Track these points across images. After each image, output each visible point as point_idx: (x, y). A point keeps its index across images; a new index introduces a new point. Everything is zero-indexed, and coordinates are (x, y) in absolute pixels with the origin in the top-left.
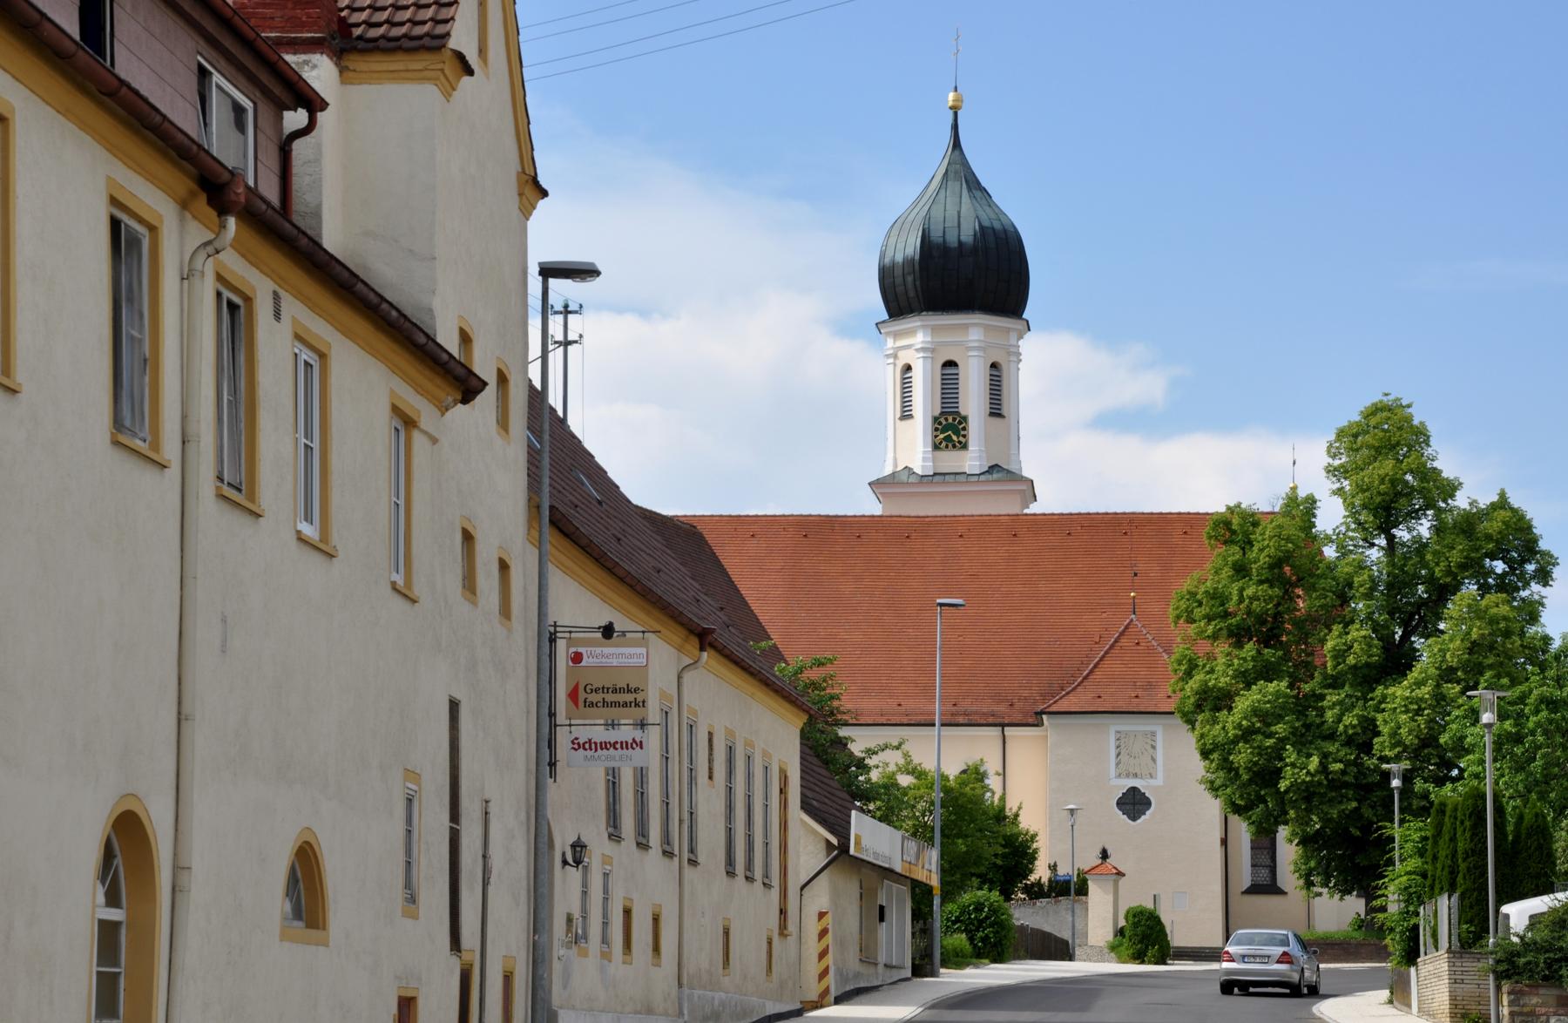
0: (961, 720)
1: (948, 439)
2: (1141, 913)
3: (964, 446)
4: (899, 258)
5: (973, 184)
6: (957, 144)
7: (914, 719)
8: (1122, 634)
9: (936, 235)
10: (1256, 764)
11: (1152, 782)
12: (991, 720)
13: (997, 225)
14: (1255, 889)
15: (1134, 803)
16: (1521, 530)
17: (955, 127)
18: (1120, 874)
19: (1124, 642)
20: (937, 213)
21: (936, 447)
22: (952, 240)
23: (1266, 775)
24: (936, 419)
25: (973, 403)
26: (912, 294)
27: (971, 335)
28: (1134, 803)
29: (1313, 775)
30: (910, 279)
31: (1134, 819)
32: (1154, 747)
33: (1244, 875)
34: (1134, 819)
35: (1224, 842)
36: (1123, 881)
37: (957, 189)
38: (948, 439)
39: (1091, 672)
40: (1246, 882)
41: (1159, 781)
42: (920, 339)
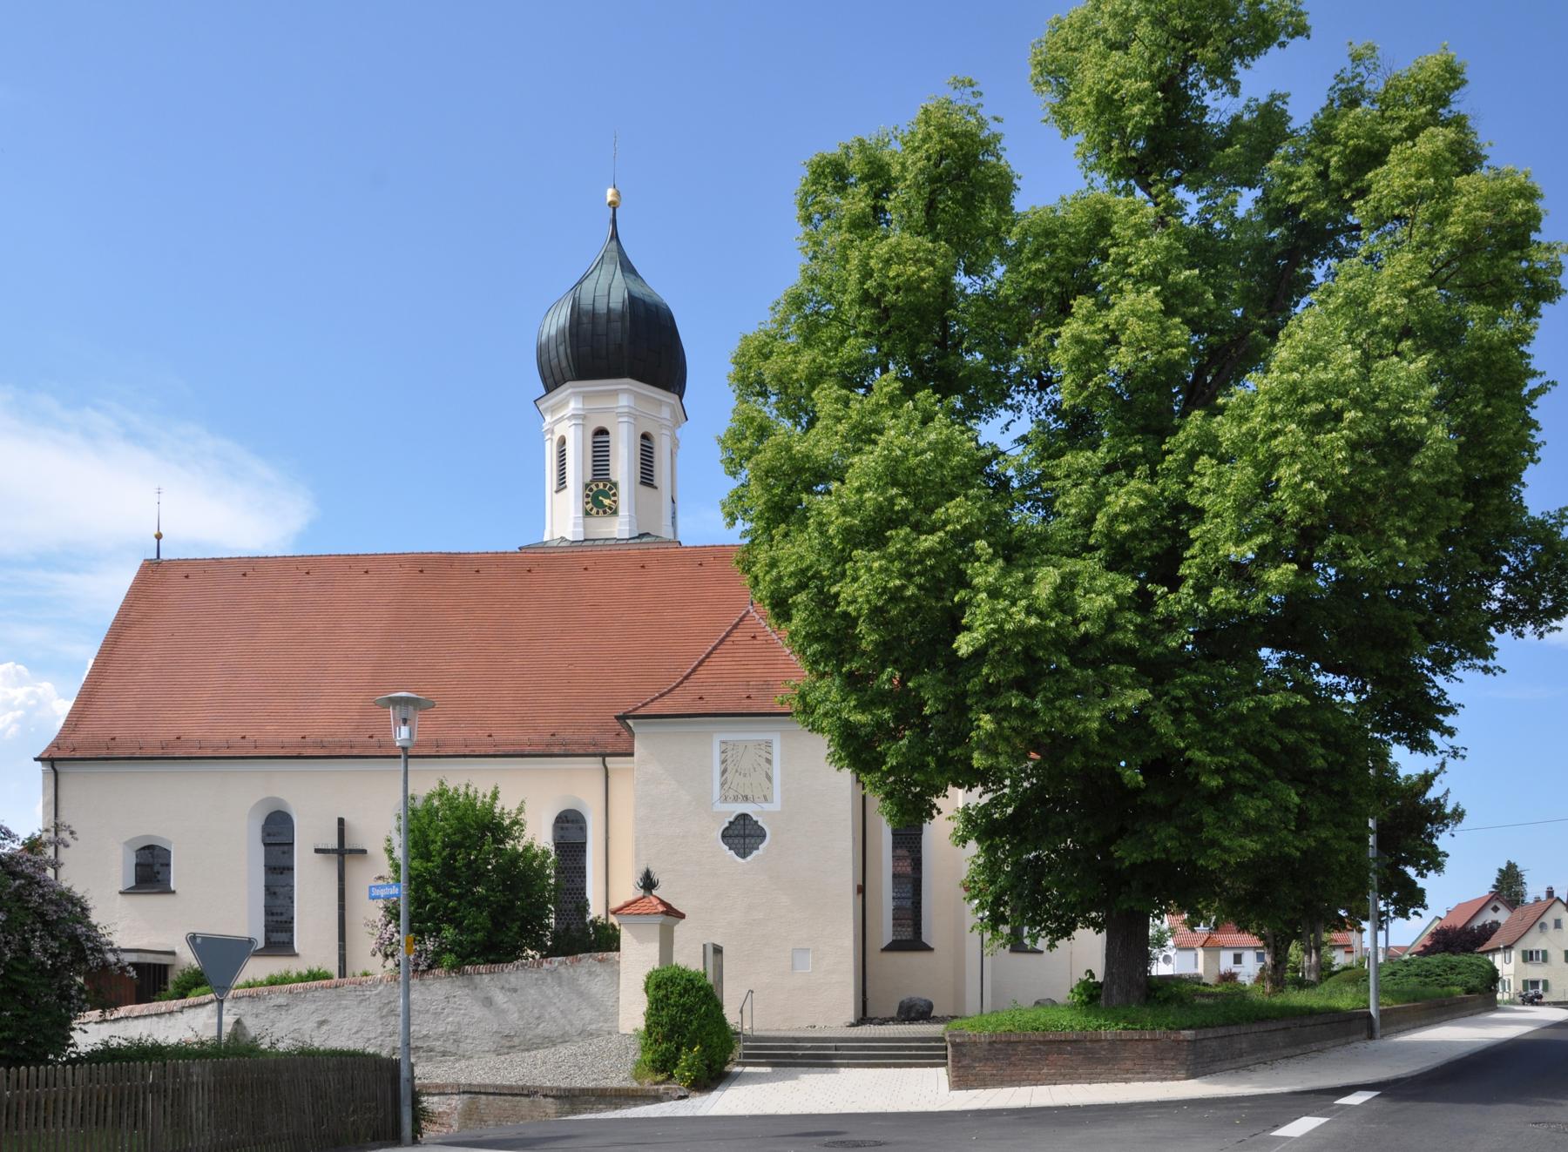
0: (556, 750)
2: (671, 979)
3: (615, 512)
4: (553, 332)
5: (628, 268)
6: (615, 236)
7: (502, 750)
8: (735, 626)
9: (586, 302)
10: (895, 596)
11: (767, 807)
12: (591, 750)
13: (647, 299)
14: (895, 946)
15: (742, 835)
17: (614, 222)
18: (672, 913)
19: (736, 636)
21: (587, 513)
22: (601, 307)
23: (921, 628)
24: (587, 486)
25: (623, 466)
26: (564, 364)
27: (622, 404)
28: (742, 835)
29: (1041, 615)
30: (562, 349)
32: (769, 761)
33: (884, 930)
34: (744, 856)
35: (862, 890)
36: (680, 929)
39: (694, 670)
40: (887, 937)
41: (775, 806)
42: (574, 406)
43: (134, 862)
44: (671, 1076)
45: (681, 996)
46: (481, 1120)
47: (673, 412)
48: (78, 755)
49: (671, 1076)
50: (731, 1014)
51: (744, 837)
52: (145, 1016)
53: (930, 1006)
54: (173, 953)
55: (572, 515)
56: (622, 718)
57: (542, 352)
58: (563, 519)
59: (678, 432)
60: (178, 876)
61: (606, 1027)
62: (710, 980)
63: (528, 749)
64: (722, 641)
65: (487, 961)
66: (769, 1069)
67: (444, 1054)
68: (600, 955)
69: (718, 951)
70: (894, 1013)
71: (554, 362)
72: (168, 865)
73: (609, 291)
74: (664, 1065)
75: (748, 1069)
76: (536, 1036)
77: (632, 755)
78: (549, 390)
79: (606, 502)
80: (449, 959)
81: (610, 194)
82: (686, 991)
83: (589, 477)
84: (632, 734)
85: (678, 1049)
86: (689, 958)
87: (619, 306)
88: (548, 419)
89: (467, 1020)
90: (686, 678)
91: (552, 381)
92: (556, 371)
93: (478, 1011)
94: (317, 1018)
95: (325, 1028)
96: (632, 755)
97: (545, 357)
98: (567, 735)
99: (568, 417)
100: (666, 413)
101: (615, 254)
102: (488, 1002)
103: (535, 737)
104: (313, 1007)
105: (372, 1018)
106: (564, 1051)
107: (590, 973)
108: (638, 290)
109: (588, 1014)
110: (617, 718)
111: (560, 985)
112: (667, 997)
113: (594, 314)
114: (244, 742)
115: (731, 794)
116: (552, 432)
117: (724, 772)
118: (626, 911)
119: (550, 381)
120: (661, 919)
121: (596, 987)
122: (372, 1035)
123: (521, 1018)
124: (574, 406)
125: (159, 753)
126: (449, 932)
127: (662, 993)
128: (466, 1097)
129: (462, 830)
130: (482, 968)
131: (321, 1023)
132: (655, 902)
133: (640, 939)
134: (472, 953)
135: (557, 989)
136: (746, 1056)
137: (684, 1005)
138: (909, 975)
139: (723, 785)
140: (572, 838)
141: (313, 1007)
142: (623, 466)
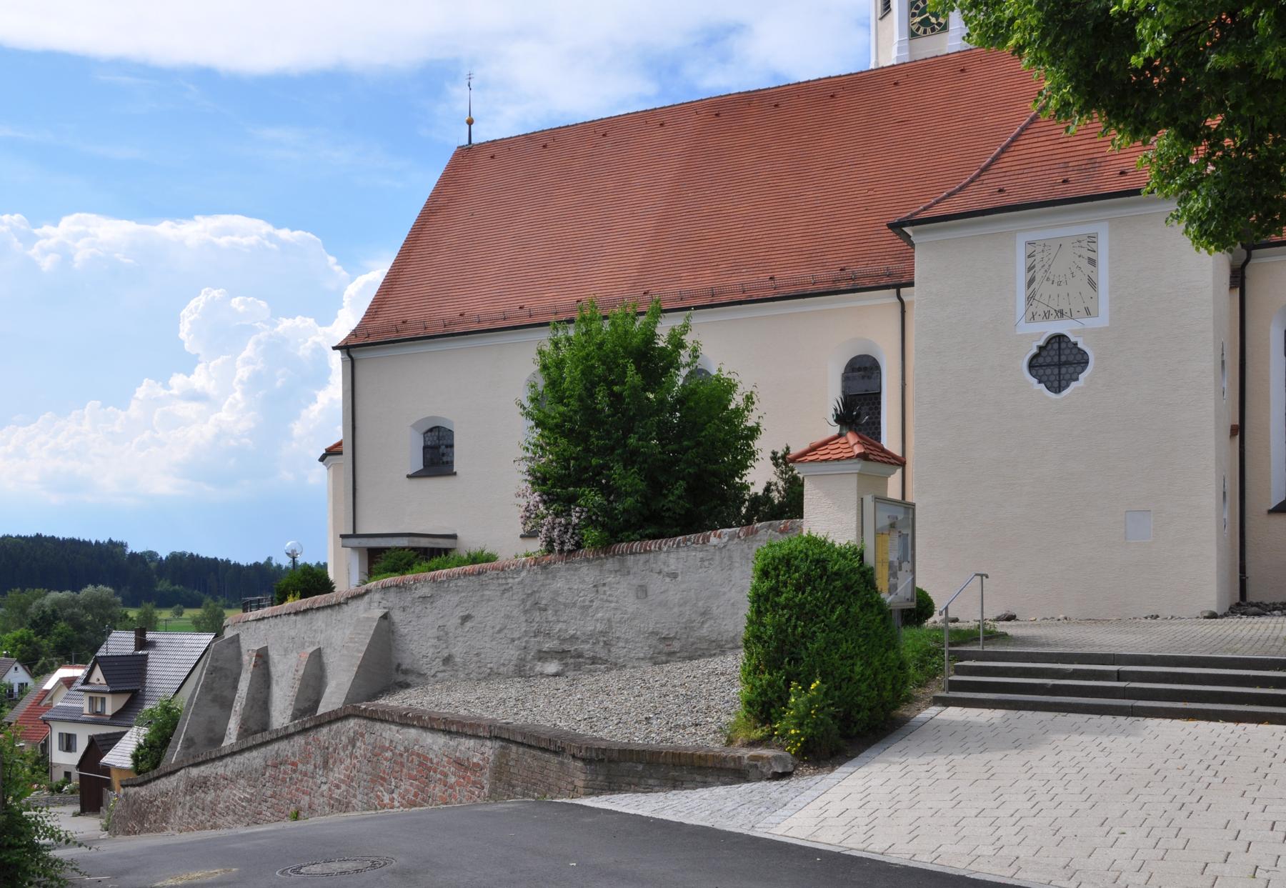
0: (843, 286)
1: (925, 22)
2: (787, 561)
11: (1089, 322)
12: (883, 282)
15: (1057, 362)
21: (913, 35)
31: (1058, 390)
32: (1092, 262)
35: (1239, 431)
38: (925, 22)
39: (996, 159)
41: (1102, 320)
43: (422, 445)
46: (510, 785)
48: (370, 341)
51: (1060, 365)
52: (323, 608)
54: (454, 537)
55: (896, 39)
56: (897, 227)
60: (461, 458)
63: (811, 288)
65: (643, 537)
67: (594, 660)
72: (452, 446)
74: (764, 708)
75: (953, 713)
76: (701, 639)
82: (809, 579)
84: (912, 245)
89: (618, 616)
94: (460, 612)
95: (468, 624)
98: (859, 268)
104: (457, 598)
105: (515, 613)
110: (892, 226)
112: (776, 591)
114: (522, 312)
115: (1041, 309)
118: (820, 454)
120: (858, 466)
122: (516, 635)
125: (440, 331)
127: (767, 584)
128: (498, 744)
131: (466, 619)
136: (954, 686)
137: (801, 606)
139: (1030, 298)
141: (457, 598)
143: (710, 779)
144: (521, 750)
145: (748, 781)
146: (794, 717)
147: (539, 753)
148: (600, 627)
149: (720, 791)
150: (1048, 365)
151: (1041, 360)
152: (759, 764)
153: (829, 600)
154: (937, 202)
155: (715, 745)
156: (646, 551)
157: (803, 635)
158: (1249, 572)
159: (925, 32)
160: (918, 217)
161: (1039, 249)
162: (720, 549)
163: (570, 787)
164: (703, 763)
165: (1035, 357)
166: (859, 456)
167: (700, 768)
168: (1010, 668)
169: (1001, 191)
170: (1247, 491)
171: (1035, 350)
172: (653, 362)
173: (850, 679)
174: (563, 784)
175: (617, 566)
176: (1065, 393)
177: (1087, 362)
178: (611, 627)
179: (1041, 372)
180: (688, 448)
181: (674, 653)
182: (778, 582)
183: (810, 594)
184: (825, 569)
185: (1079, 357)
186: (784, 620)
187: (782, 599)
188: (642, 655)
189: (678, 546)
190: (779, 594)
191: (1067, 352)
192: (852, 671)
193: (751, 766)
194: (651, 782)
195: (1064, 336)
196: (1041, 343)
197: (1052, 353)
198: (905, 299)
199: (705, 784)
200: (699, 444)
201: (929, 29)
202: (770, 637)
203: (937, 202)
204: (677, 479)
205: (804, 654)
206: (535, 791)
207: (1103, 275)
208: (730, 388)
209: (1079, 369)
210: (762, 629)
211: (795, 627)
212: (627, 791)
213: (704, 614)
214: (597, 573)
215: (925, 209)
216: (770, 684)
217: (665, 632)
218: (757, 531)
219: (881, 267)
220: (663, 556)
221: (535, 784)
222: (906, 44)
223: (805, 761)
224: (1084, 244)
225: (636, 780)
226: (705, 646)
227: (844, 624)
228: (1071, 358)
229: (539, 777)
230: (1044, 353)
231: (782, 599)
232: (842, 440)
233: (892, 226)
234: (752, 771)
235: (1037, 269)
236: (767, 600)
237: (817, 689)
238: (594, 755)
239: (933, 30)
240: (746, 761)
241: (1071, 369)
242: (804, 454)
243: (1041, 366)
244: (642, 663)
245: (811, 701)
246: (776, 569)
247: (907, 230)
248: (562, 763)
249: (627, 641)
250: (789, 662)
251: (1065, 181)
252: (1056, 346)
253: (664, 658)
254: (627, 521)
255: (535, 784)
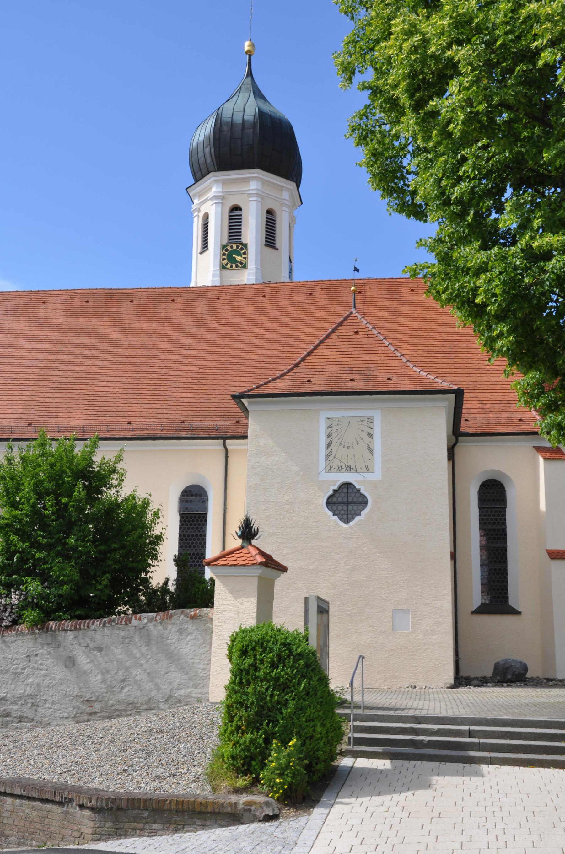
0: (184, 434)
2: (262, 643)
3: (245, 266)
4: (201, 139)
5: (258, 94)
6: (250, 74)
8: (340, 324)
9: (227, 116)
11: (369, 476)
12: (214, 434)
13: (273, 114)
14: (482, 610)
16: (332, 756)
18: (269, 562)
19: (341, 331)
20: (228, 107)
21: (223, 267)
22: (238, 119)
24: (224, 247)
25: (252, 232)
26: (209, 160)
27: (253, 188)
28: (346, 502)
30: (207, 150)
32: (370, 435)
33: (475, 596)
34: (347, 521)
35: (453, 556)
36: (281, 582)
37: (247, 94)
39: (303, 359)
41: (377, 475)
42: (215, 190)
44: (256, 781)
45: (274, 665)
47: (292, 196)
49: (256, 781)
50: (337, 682)
51: (347, 504)
53: (525, 668)
55: (212, 268)
56: (237, 398)
57: (193, 155)
58: (205, 271)
59: (295, 213)
61: (196, 693)
62: (313, 644)
63: (159, 434)
64: (328, 336)
66: (384, 764)
68: (192, 612)
69: (323, 610)
70: (489, 672)
71: (202, 160)
73: (245, 108)
74: (248, 764)
75: (362, 763)
76: (119, 702)
77: (245, 437)
78: (197, 180)
79: (238, 258)
80: (31, 615)
81: (247, 46)
83: (226, 241)
85: (267, 741)
86: (289, 618)
87: (252, 118)
88: (196, 201)
89: (47, 681)
90: (297, 365)
91: (199, 173)
92: (203, 167)
93: (60, 672)
96: (245, 437)
97: (195, 157)
98: (195, 422)
99: (210, 200)
100: (286, 195)
101: (250, 86)
102: (70, 662)
103: (168, 424)
106: (144, 722)
107: (181, 631)
108: (266, 108)
109: (176, 677)
110: (234, 397)
111: (148, 644)
113: (232, 124)
115: (336, 463)
116: (199, 211)
117: (329, 445)
118: (229, 560)
119: (198, 175)
120: (259, 571)
121: (186, 647)
123: (104, 681)
124: (215, 190)
126: (34, 586)
127: (249, 661)
129: (56, 477)
130: (68, 624)
132: (254, 552)
133: (236, 594)
134: (59, 608)
135: (144, 649)
137: (277, 679)
138: (504, 637)
139: (328, 456)
140: (195, 508)
142: (252, 232)
143: (208, 823)
144: (17, 802)
145: (242, 823)
146: (276, 768)
147: (38, 804)
148: (29, 690)
149: (219, 831)
150: (340, 503)
151: (335, 499)
152: (253, 808)
153: (295, 675)
154: (266, 383)
155: (202, 791)
156: (76, 629)
157: (278, 702)
158: (460, 655)
159: (231, 267)
160: (252, 393)
161: (335, 423)
162: (140, 629)
163: (76, 834)
164: (203, 809)
165: (331, 497)
166: (261, 564)
167: (200, 813)
168: (391, 728)
169: (309, 381)
170: (458, 598)
171: (331, 492)
172: (96, 480)
173: (312, 737)
174: (67, 832)
175: (49, 640)
176: (352, 523)
177: (366, 503)
178: (40, 691)
179: (335, 508)
180: (115, 550)
181: (95, 713)
182: (255, 659)
183: (282, 670)
184: (290, 651)
185: (361, 499)
186: (263, 690)
187: (261, 673)
188: (66, 715)
189: (105, 623)
190: (256, 669)
191: (353, 495)
192: (314, 731)
193: (245, 810)
194: (155, 826)
195: (351, 484)
196: (336, 487)
197: (343, 495)
198: (229, 448)
199: (204, 827)
200: (123, 547)
201: (234, 266)
202: (252, 703)
203: (266, 383)
204: (104, 573)
205: (279, 717)
206: (32, 839)
207: (377, 444)
208: (146, 504)
209: (360, 507)
210: (244, 697)
211: (272, 696)
212: (133, 836)
213: (123, 681)
214: (31, 645)
215: (257, 387)
216: (252, 741)
217: (88, 696)
218: (171, 616)
219: (211, 424)
220: (91, 633)
221: (33, 833)
222: (218, 272)
223: (286, 805)
224: (365, 423)
225: (141, 825)
226: (122, 707)
227: (308, 694)
228: (355, 500)
229: (39, 826)
230: (337, 495)
231: (261, 673)
232: (244, 551)
233: (234, 397)
234: (246, 814)
235: (334, 436)
236: (248, 673)
237: (294, 746)
238: (104, 804)
239: (237, 266)
240: (240, 807)
241: (355, 507)
242: (216, 559)
243: (334, 503)
244: (66, 722)
245: (289, 755)
246: (253, 649)
247: (245, 401)
248: (67, 813)
249: (53, 703)
250: (268, 724)
251: (352, 380)
252: (345, 490)
253: (86, 718)
254: (59, 604)
255: (33, 833)
